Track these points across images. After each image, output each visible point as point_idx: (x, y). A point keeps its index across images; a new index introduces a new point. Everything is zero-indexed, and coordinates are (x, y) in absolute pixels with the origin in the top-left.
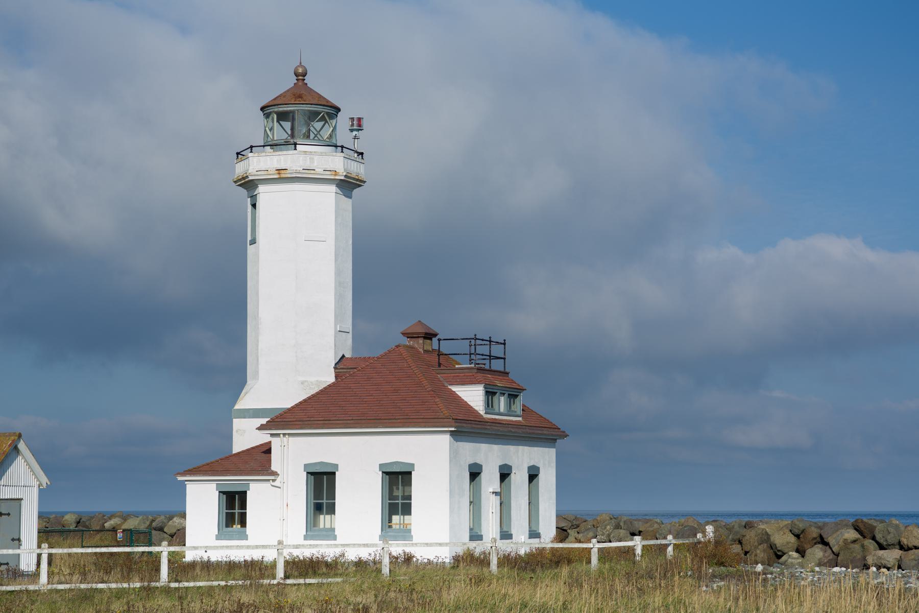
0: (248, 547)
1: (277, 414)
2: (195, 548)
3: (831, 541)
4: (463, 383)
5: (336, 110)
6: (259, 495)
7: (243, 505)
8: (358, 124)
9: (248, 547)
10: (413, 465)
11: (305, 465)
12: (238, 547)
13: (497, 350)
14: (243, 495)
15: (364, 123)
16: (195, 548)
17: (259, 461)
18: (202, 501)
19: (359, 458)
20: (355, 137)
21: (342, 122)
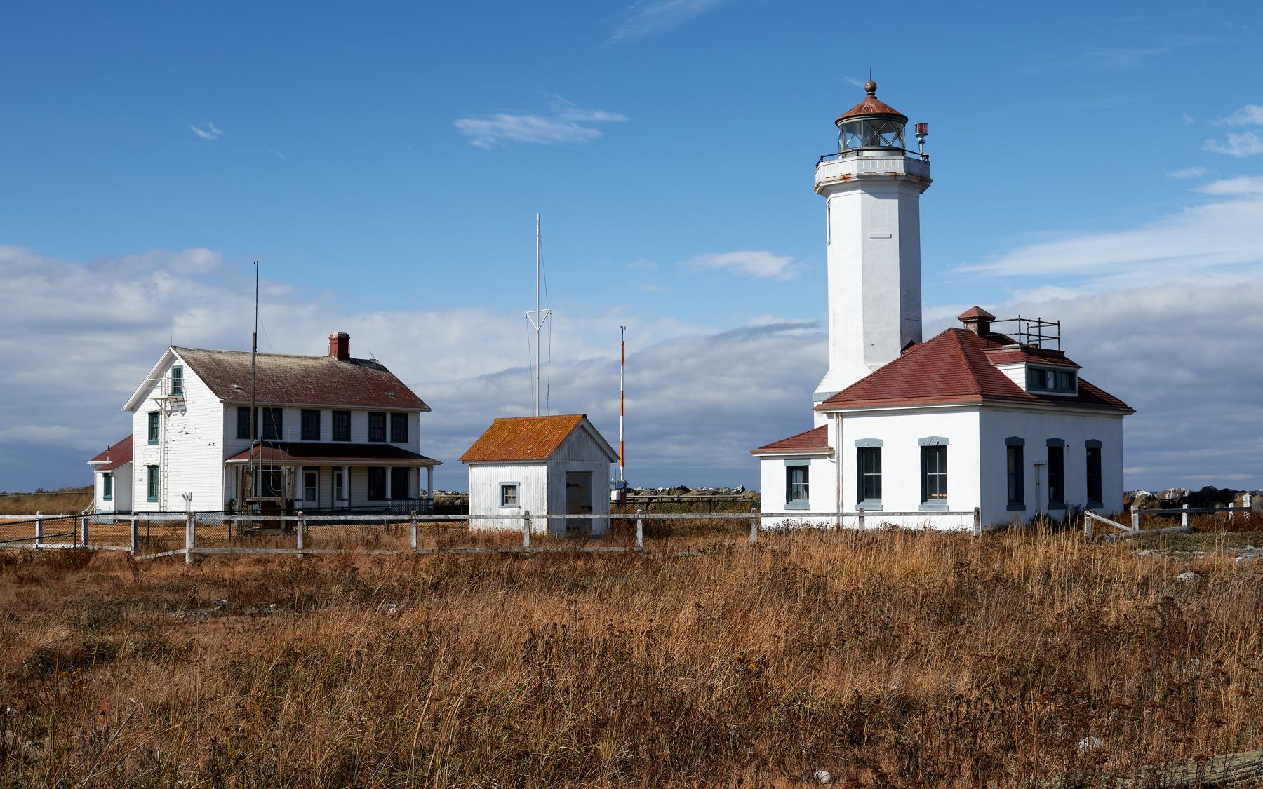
0: (809, 515)
1: (828, 397)
2: (771, 515)
3: (867, 519)
4: (1007, 363)
5: (903, 119)
6: (820, 472)
7: (806, 479)
8: (922, 130)
9: (809, 515)
10: (947, 439)
11: (1048, 441)
12: (801, 515)
13: (1047, 331)
14: (805, 469)
15: (929, 130)
16: (771, 515)
17: (816, 440)
18: (773, 475)
19: (901, 435)
20: (922, 142)
21: (909, 130)
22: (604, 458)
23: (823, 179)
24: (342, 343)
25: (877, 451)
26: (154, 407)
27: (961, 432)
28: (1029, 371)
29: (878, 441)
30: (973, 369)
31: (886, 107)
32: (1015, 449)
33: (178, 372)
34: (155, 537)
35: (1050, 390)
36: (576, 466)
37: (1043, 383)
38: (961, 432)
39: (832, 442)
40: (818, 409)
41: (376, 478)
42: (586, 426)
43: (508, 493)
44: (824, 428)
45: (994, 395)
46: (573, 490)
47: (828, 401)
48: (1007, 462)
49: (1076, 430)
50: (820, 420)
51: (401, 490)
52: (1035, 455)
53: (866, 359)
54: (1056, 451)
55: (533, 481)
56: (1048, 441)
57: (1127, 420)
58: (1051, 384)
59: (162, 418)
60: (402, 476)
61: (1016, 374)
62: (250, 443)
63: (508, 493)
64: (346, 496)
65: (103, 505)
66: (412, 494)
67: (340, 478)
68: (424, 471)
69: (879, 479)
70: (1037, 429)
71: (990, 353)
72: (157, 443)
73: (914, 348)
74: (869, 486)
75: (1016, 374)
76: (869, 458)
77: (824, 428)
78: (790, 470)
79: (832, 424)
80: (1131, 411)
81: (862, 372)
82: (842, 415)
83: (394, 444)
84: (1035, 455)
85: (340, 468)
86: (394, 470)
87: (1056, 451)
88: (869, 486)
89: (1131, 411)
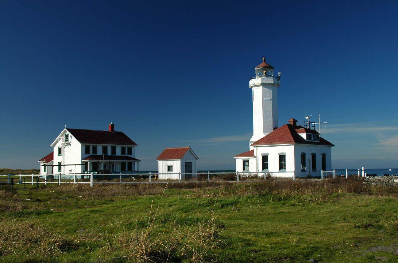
6: (252, 161)
10: (286, 153)
11: (322, 154)
14: (248, 161)
18: (239, 162)
19: (273, 152)
22: (195, 159)
23: (252, 84)
24: (113, 126)
25: (267, 156)
26: (60, 145)
27: (289, 151)
28: (307, 135)
29: (267, 154)
30: (293, 135)
31: (270, 65)
32: (303, 156)
33: (67, 136)
34: (67, 181)
35: (312, 140)
36: (188, 161)
37: (310, 139)
38: (289, 151)
39: (255, 154)
40: (251, 145)
41: (123, 165)
42: (191, 150)
43: (170, 168)
44: (253, 151)
45: (298, 140)
46: (187, 167)
47: (255, 143)
48: (301, 159)
49: (318, 150)
50: (251, 148)
51: (130, 169)
52: (309, 157)
53: (264, 132)
54: (314, 156)
55: (177, 165)
56: (322, 154)
57: (332, 147)
58: (312, 139)
59: (62, 149)
60: (130, 165)
61: (304, 135)
62: (88, 155)
63: (170, 168)
64: (115, 170)
65: (43, 174)
66: (133, 170)
67: (113, 165)
68: (136, 163)
69: (268, 164)
70: (309, 150)
71: (297, 130)
72: (61, 155)
73: (276, 129)
74: (265, 165)
75: (304, 135)
76: (265, 159)
77: (253, 151)
78: (244, 162)
79: (255, 149)
80: (333, 145)
81: (262, 135)
82: (258, 147)
83: (129, 156)
84: (309, 157)
85: (113, 162)
86: (128, 163)
87: (314, 156)
88: (265, 165)
89: (333, 145)
